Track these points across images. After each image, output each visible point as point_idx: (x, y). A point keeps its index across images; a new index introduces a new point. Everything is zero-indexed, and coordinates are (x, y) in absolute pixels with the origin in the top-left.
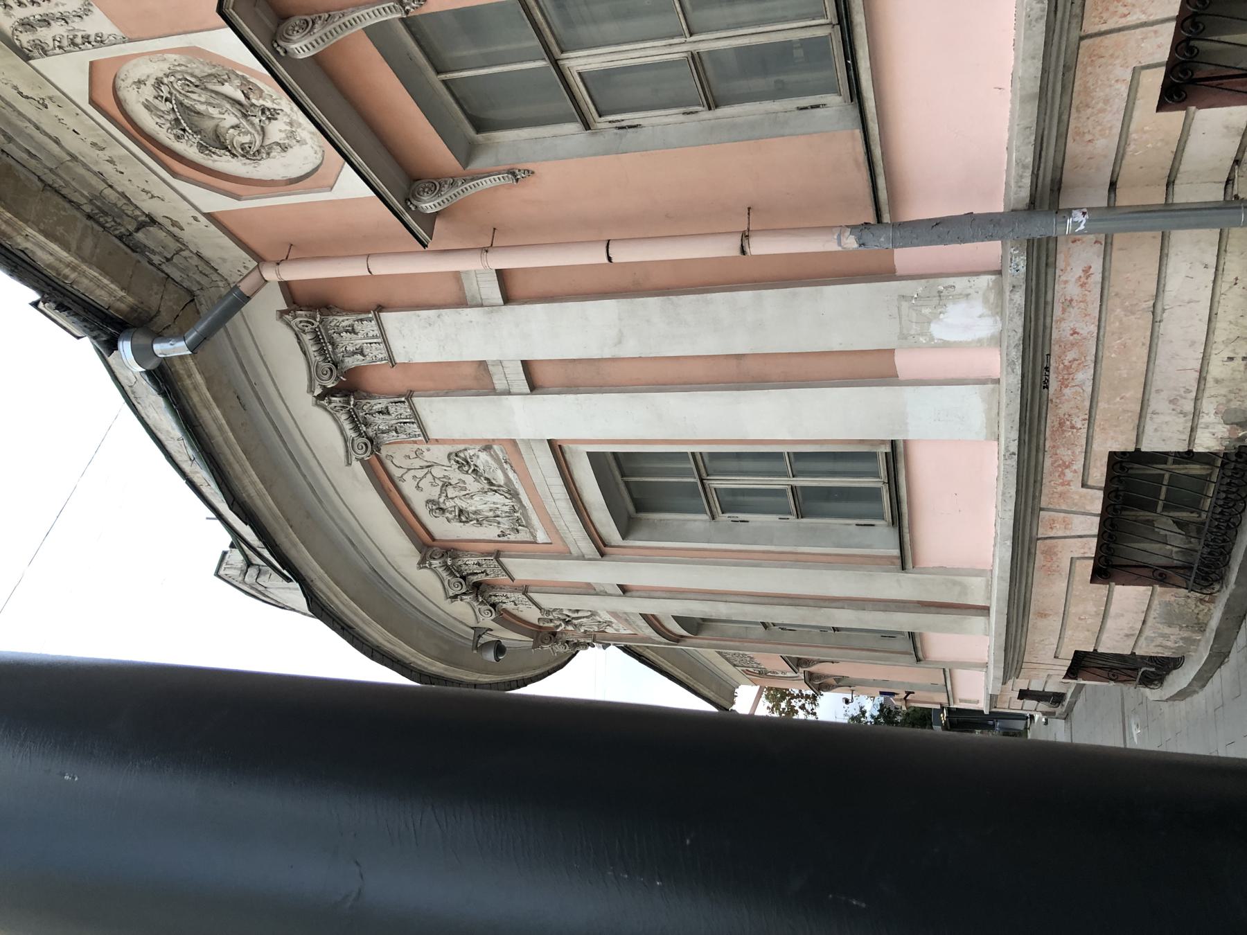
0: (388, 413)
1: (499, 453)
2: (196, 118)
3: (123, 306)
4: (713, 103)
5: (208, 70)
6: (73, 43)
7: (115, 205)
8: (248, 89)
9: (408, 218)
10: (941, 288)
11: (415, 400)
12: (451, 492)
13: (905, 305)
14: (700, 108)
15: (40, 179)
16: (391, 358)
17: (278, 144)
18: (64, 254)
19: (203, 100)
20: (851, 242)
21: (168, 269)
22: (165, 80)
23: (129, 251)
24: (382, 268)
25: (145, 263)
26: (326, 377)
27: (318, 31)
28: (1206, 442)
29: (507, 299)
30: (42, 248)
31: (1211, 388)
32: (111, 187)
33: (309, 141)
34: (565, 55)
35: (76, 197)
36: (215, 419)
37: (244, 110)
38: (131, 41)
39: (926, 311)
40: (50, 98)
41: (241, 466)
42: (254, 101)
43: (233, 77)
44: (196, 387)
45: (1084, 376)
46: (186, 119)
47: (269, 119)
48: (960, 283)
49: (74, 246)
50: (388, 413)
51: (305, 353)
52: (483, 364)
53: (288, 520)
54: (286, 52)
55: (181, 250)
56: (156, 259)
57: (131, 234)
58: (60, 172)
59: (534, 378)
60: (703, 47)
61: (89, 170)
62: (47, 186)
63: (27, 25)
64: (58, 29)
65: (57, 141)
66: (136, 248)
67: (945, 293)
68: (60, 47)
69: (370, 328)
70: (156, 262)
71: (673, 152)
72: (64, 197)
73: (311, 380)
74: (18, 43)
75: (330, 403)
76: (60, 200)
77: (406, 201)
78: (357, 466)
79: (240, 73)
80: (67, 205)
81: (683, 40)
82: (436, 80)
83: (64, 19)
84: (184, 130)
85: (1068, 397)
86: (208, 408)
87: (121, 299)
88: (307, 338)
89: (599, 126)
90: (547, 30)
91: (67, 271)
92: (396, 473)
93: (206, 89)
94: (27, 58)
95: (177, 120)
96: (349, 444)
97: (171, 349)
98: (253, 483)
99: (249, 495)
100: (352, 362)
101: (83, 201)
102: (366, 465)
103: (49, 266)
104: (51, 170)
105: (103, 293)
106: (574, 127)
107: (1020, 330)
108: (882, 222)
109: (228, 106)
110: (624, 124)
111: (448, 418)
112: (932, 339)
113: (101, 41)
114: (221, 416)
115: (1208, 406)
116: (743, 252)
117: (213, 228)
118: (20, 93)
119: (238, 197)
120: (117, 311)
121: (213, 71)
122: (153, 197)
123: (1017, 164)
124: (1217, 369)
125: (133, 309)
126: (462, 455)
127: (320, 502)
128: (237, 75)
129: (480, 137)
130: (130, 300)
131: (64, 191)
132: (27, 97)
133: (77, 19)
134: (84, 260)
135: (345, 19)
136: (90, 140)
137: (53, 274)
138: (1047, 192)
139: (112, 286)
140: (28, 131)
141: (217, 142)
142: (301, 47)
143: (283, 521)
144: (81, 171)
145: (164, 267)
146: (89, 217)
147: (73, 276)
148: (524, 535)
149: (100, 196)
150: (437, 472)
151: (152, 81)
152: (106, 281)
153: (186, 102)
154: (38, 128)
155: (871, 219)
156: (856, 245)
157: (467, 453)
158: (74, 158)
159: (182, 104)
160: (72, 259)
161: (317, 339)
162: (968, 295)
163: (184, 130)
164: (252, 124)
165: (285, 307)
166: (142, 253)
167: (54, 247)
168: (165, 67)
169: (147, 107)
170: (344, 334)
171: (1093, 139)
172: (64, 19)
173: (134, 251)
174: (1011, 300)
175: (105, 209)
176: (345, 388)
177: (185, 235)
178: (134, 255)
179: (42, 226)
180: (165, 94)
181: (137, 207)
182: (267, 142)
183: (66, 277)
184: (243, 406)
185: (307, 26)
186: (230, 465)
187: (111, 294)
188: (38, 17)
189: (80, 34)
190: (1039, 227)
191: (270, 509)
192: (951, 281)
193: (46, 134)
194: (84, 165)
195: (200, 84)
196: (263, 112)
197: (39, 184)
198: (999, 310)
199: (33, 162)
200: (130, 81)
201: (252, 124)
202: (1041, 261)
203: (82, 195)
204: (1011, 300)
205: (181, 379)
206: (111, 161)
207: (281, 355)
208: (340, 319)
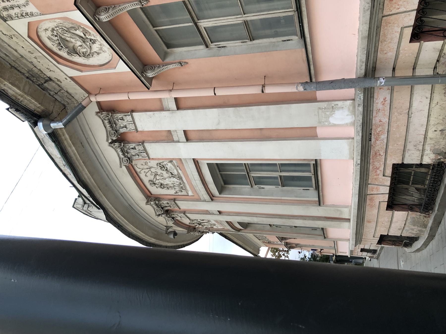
0: (135, 149)
2: (66, 43)
3: (39, 110)
4: (252, 39)
5: (71, 25)
6: (22, 15)
10: (333, 105)
11: (145, 144)
12: (158, 177)
13: (320, 111)
15: (10, 64)
17: (96, 52)
18: (18, 91)
20: (301, 89)
21: (56, 97)
22: (55, 29)
25: (48, 95)
27: (111, 12)
28: (427, 160)
29: (178, 108)
30: (10, 89)
31: (428, 140)
32: (35, 67)
34: (199, 21)
35: (23, 71)
36: (73, 151)
38: (43, 15)
39: (328, 113)
40: (14, 35)
41: (82, 167)
42: (87, 37)
43: (80, 28)
44: (66, 139)
45: (384, 137)
46: (63, 43)
48: (340, 103)
49: (22, 88)
50: (135, 149)
52: (169, 131)
53: (99, 187)
54: (99, 19)
55: (61, 90)
56: (52, 93)
57: (42, 84)
60: (249, 19)
61: (28, 61)
62: (12, 67)
64: (17, 10)
65: (16, 51)
67: (335, 107)
69: (129, 118)
70: (52, 94)
72: (18, 71)
73: (107, 137)
74: (2, 15)
75: (114, 145)
77: (94, 15)
78: (124, 168)
80: (20, 74)
81: (241, 16)
83: (19, 7)
84: (62, 47)
85: (378, 144)
86: (70, 147)
87: (39, 107)
88: (106, 122)
89: (212, 47)
90: (193, 12)
91: (19, 97)
92: (138, 170)
94: (5, 21)
95: (59, 43)
96: (121, 160)
98: (86, 174)
99: (85, 178)
100: (122, 131)
102: (127, 168)
103: (13, 95)
106: (202, 47)
107: (361, 120)
108: (312, 82)
109: (78, 38)
110: (220, 46)
113: (32, 15)
115: (428, 148)
116: (263, 92)
117: (72, 82)
120: (37, 112)
121: (73, 26)
122: (51, 71)
123: (360, 61)
124: (431, 134)
125: (43, 111)
126: (162, 164)
128: (81, 27)
130: (42, 108)
131: (18, 69)
132: (5, 35)
133: (23, 7)
134: (25, 93)
135: (120, 8)
137: (14, 98)
138: (371, 71)
139: (36, 103)
141: (74, 51)
142: (104, 17)
145: (54, 96)
146: (27, 78)
147: (22, 99)
148: (184, 193)
149: (32, 70)
150: (153, 170)
151: (50, 29)
152: (33, 101)
153: (63, 37)
154: (9, 46)
155: (308, 80)
156: (303, 90)
158: (22, 56)
159: (61, 37)
161: (110, 122)
162: (343, 108)
163: (62, 47)
164: (87, 45)
165: (98, 111)
166: (47, 91)
168: (55, 24)
169: (48, 38)
170: (119, 120)
171: (387, 52)
172: (19, 7)
173: (43, 90)
174: (358, 109)
176: (120, 140)
177: (63, 85)
179: (10, 81)
180: (55, 34)
181: (45, 74)
182: (92, 51)
184: (83, 146)
185: (107, 10)
186: (78, 167)
189: (24, 12)
190: (368, 84)
191: (92, 183)
193: (12, 48)
196: (91, 41)
197: (9, 66)
199: (7, 58)
200: (42, 29)
201: (87, 45)
202: (369, 96)
204: (358, 109)
205: (60, 137)
206: (35, 58)
207: (97, 128)
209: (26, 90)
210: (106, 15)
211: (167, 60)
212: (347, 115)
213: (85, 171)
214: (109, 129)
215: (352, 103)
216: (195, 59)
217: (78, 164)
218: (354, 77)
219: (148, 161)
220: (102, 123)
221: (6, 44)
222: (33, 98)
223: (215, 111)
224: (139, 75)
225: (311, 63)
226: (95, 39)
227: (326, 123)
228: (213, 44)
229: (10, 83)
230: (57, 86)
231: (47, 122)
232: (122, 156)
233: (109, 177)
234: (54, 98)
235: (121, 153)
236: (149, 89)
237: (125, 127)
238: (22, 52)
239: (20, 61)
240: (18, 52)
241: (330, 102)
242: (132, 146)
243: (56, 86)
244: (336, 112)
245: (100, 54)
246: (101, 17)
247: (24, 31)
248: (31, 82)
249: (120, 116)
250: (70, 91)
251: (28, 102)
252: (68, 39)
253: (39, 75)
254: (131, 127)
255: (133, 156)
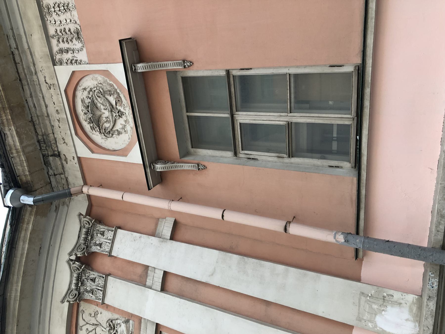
0: (94, 282)
1: (131, 326)
2: (95, 109)
3: (24, 179)
4: (290, 155)
7: (50, 142)
8: (119, 100)
9: (148, 170)
10: (385, 294)
11: (110, 278)
13: (363, 298)
14: (285, 156)
15: (32, 117)
16: (111, 251)
17: (117, 130)
18: (18, 144)
19: (101, 102)
20: (341, 238)
21: (53, 179)
23: (43, 163)
24: (130, 198)
25: (46, 172)
26: (80, 250)
30: (12, 137)
32: (53, 133)
33: (129, 132)
35: (39, 131)
36: (23, 249)
37: (112, 109)
39: (375, 307)
41: (18, 278)
42: (118, 107)
43: (115, 93)
44: (26, 230)
46: (92, 107)
47: (119, 115)
48: (397, 295)
49: (24, 144)
50: (94, 282)
51: (79, 237)
52: (147, 267)
53: (18, 321)
54: (154, 168)
55: (62, 174)
56: (51, 172)
57: (48, 156)
58: (40, 118)
59: (167, 283)
60: (294, 120)
61: (50, 123)
62: (32, 121)
63: (61, 51)
64: (69, 56)
65: (46, 107)
66: (47, 163)
67: (387, 298)
68: (66, 63)
69: (110, 235)
70: (50, 174)
71: (267, 172)
72: (35, 129)
73: (73, 250)
74: (55, 58)
75: (73, 264)
76: (33, 128)
78: (66, 304)
79: (118, 91)
80: (34, 132)
81: (286, 114)
82: (185, 114)
84: (88, 111)
86: (24, 242)
87: (26, 176)
88: (84, 230)
89: (241, 156)
90: (234, 98)
91: (14, 151)
92: (81, 322)
93: (104, 96)
94: (54, 64)
95: (88, 106)
96: (69, 292)
97: (27, 200)
98: (16, 290)
99: (10, 296)
100: (95, 249)
101: (40, 133)
102: (71, 307)
103: (9, 145)
104: (37, 116)
105: (21, 168)
106: (230, 154)
107: (431, 328)
108: (361, 236)
109: (108, 105)
110: (251, 157)
111: (120, 294)
112: (376, 326)
114: (26, 249)
116: (285, 230)
117: (77, 165)
118: (45, 80)
119: (93, 152)
120: (21, 180)
122: (64, 142)
123: (438, 213)
125: (27, 183)
126: (114, 322)
127: (39, 323)
128: (117, 92)
129: (192, 150)
130: (29, 178)
131: (37, 127)
132: (47, 83)
134: (23, 151)
136: (57, 108)
137: (8, 148)
139: (26, 168)
140: (39, 98)
141: (96, 122)
143: (15, 320)
144: (47, 122)
145: (51, 177)
146: (39, 141)
147: (15, 155)
149: (48, 135)
152: (25, 164)
153: (96, 101)
154: (43, 98)
155: (353, 231)
156: (343, 241)
157: (116, 321)
158: (48, 116)
159: (93, 102)
160: (19, 147)
161: (87, 233)
162: (400, 304)
164: (112, 116)
165: (84, 213)
166: (47, 166)
167: (17, 139)
168: (95, 83)
169: (82, 101)
170: (99, 235)
173: (45, 164)
174: (427, 305)
175: (46, 141)
176: (85, 260)
177: (67, 166)
178: (44, 166)
179: (18, 130)
180: (90, 96)
181: (57, 146)
182: (115, 129)
183: (12, 153)
184: (40, 253)
185: (165, 163)
186: (14, 275)
187: (23, 171)
188: (66, 48)
189: (75, 59)
191: (14, 309)
192: (391, 292)
194: (50, 120)
195: (103, 94)
196: (118, 112)
197: (30, 119)
198: (418, 319)
199: (34, 109)
200: (82, 88)
201: (112, 116)
203: (42, 131)
204: (427, 305)
205: (23, 223)
206: (59, 121)
208: (102, 227)
209: (27, 150)
210: (162, 166)
211: (186, 159)
212: (407, 320)
213: (17, 286)
214: (82, 241)
215: (417, 299)
216: (218, 166)
217: (16, 271)
218: (425, 245)
219: (99, 309)
220: (78, 230)
221: (41, 95)
222: (28, 160)
223: (216, 252)
224: (147, 163)
225: (363, 205)
226: (124, 111)
227: (370, 325)
228: (244, 152)
229: (17, 133)
230: (61, 166)
231: (18, 192)
232: (73, 287)
233: (40, 317)
234: (50, 179)
235: (74, 282)
236: (149, 189)
237: (100, 245)
238: (52, 110)
239: (43, 119)
240: (48, 108)
241: (380, 289)
242: (93, 275)
243: (60, 167)
244: (389, 308)
245: (121, 135)
246: (157, 166)
247: (63, 83)
248: (39, 148)
249: (102, 228)
250: (70, 179)
251: (19, 162)
252: (99, 105)
253: (51, 144)
254: (106, 248)
255: (87, 292)
